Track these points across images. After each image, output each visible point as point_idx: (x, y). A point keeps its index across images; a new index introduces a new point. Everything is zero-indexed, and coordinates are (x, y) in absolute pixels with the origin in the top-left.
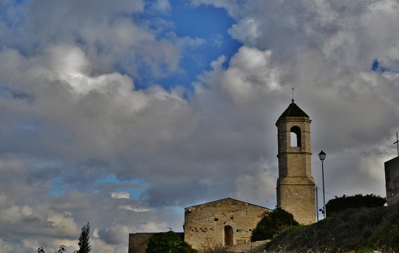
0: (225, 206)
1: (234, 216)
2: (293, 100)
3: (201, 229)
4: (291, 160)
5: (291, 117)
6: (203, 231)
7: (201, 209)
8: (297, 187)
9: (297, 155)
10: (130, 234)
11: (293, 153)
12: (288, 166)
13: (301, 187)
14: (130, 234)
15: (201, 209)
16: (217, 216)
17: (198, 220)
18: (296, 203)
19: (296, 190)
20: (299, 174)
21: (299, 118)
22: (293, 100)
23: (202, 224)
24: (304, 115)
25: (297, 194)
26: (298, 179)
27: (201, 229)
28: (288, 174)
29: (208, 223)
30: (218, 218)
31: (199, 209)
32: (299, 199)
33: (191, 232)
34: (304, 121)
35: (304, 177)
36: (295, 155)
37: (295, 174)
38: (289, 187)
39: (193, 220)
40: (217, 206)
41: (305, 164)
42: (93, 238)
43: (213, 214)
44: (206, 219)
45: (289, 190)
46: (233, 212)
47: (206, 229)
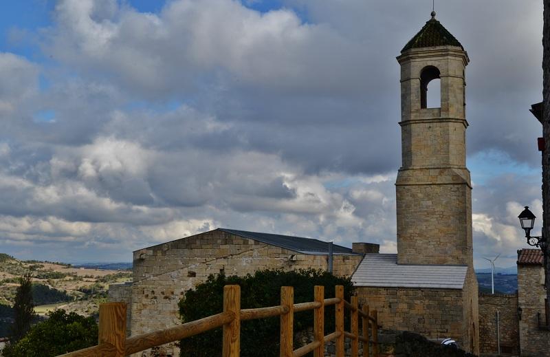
0: (209, 246)
1: (226, 267)
2: (433, 14)
3: (163, 293)
4: (418, 135)
5: (420, 49)
6: (166, 298)
7: (164, 253)
8: (429, 189)
9: (431, 125)
10: (379, 245)
11: (423, 121)
12: (413, 148)
13: (437, 189)
14: (379, 245)
15: (164, 253)
16: (193, 267)
17: (157, 275)
18: (427, 221)
19: (428, 196)
20: (433, 162)
21: (438, 48)
22: (433, 14)
23: (164, 283)
24: (452, 41)
25: (430, 203)
26: (432, 172)
27: (163, 293)
28: (413, 163)
29: (176, 280)
30: (196, 272)
31: (159, 254)
32: (434, 213)
33: (145, 301)
34: (448, 55)
35: (443, 169)
36: (427, 125)
37: (427, 164)
38: (414, 190)
39: (147, 276)
40: (193, 246)
41: (448, 143)
42: (321, 230)
43: (186, 263)
44: (173, 273)
45: (413, 196)
46: (224, 258)
47: (172, 293)
